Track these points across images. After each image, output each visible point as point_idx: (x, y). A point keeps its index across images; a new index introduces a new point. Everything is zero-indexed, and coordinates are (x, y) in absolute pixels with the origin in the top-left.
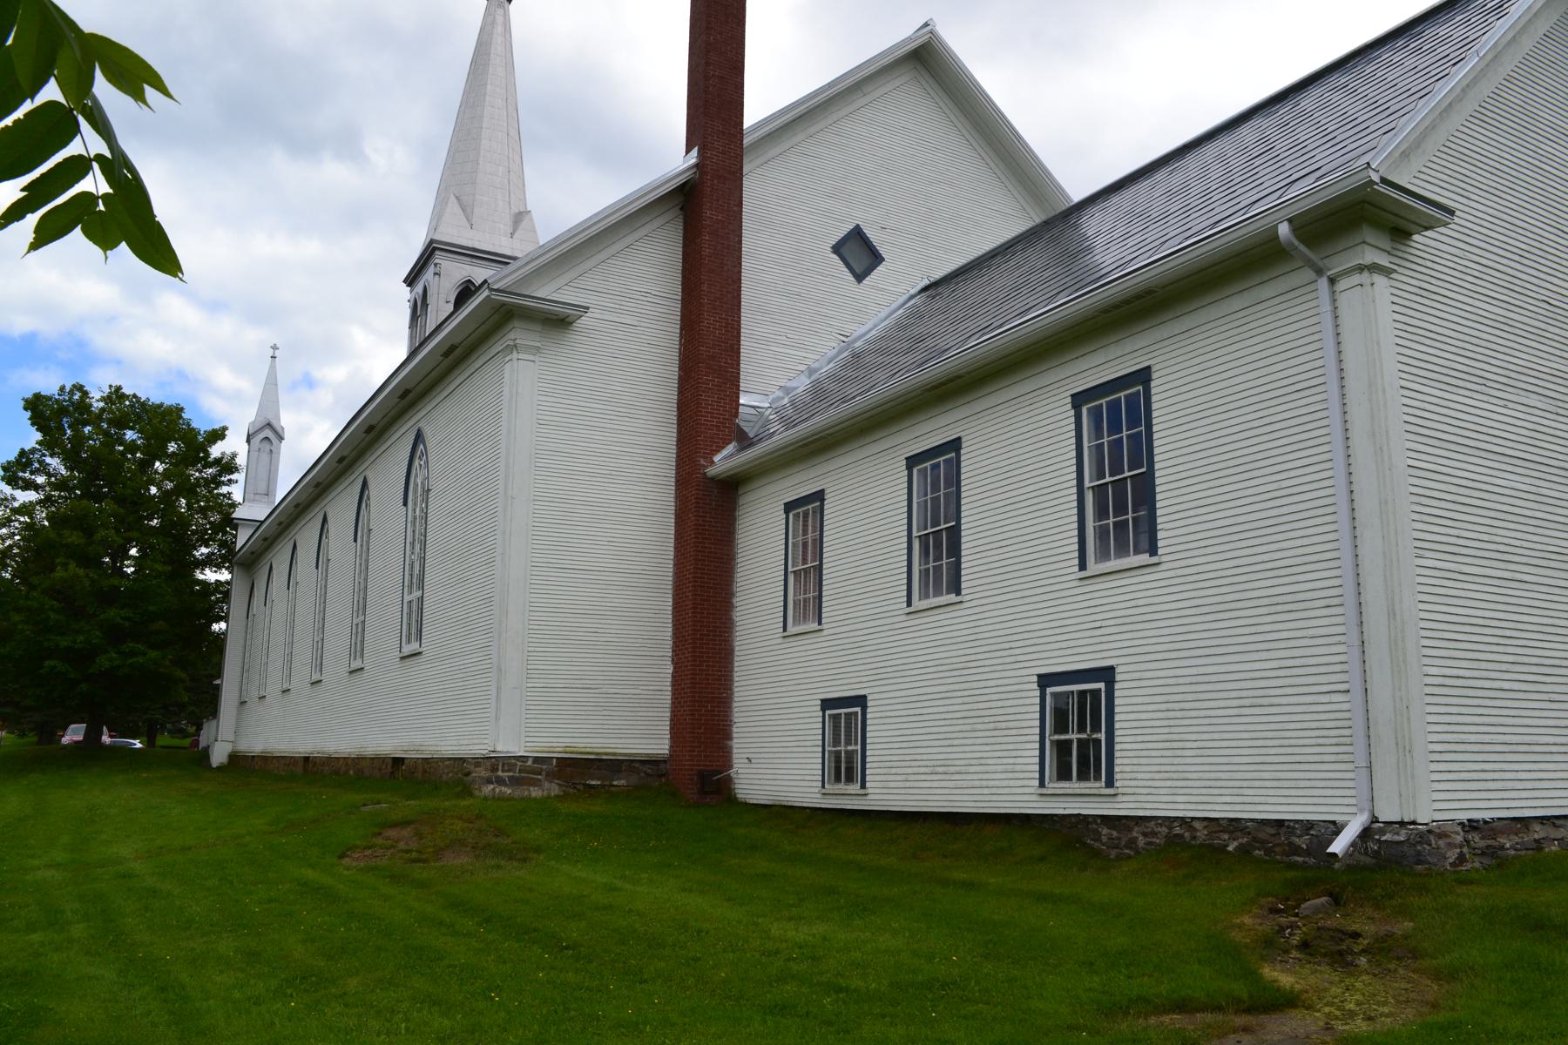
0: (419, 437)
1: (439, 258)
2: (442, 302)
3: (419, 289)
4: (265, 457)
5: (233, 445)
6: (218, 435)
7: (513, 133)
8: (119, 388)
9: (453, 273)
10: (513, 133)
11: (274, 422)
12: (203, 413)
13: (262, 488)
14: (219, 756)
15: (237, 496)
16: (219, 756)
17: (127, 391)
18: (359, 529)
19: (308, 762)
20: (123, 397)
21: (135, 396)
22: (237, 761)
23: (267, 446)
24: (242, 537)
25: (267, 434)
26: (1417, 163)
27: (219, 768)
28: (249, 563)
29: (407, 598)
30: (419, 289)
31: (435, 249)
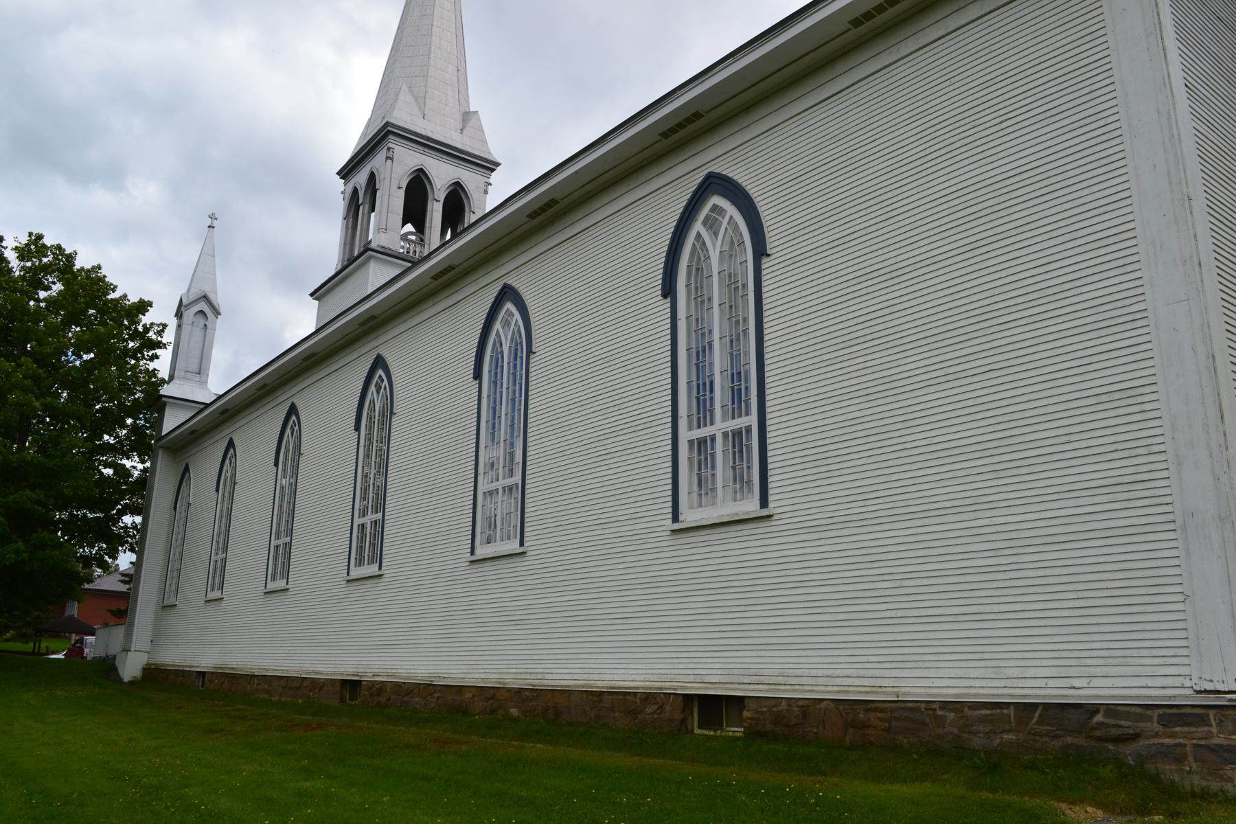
0: (231, 444)
1: (392, 142)
2: (394, 187)
3: (361, 178)
4: (198, 333)
5: (160, 314)
6: (143, 306)
7: (460, 36)
8: (40, 237)
9: (406, 160)
10: (460, 36)
11: (211, 295)
12: (127, 285)
13: (194, 365)
14: (130, 668)
15: (164, 373)
16: (130, 668)
17: (48, 241)
18: (226, 484)
19: (351, 686)
20: (42, 250)
21: (59, 247)
22: (155, 675)
23: (201, 321)
24: (172, 421)
25: (200, 309)
26: (351, 573)
27: (133, 683)
28: (184, 445)
29: (357, 521)
30: (361, 178)
31: (390, 132)
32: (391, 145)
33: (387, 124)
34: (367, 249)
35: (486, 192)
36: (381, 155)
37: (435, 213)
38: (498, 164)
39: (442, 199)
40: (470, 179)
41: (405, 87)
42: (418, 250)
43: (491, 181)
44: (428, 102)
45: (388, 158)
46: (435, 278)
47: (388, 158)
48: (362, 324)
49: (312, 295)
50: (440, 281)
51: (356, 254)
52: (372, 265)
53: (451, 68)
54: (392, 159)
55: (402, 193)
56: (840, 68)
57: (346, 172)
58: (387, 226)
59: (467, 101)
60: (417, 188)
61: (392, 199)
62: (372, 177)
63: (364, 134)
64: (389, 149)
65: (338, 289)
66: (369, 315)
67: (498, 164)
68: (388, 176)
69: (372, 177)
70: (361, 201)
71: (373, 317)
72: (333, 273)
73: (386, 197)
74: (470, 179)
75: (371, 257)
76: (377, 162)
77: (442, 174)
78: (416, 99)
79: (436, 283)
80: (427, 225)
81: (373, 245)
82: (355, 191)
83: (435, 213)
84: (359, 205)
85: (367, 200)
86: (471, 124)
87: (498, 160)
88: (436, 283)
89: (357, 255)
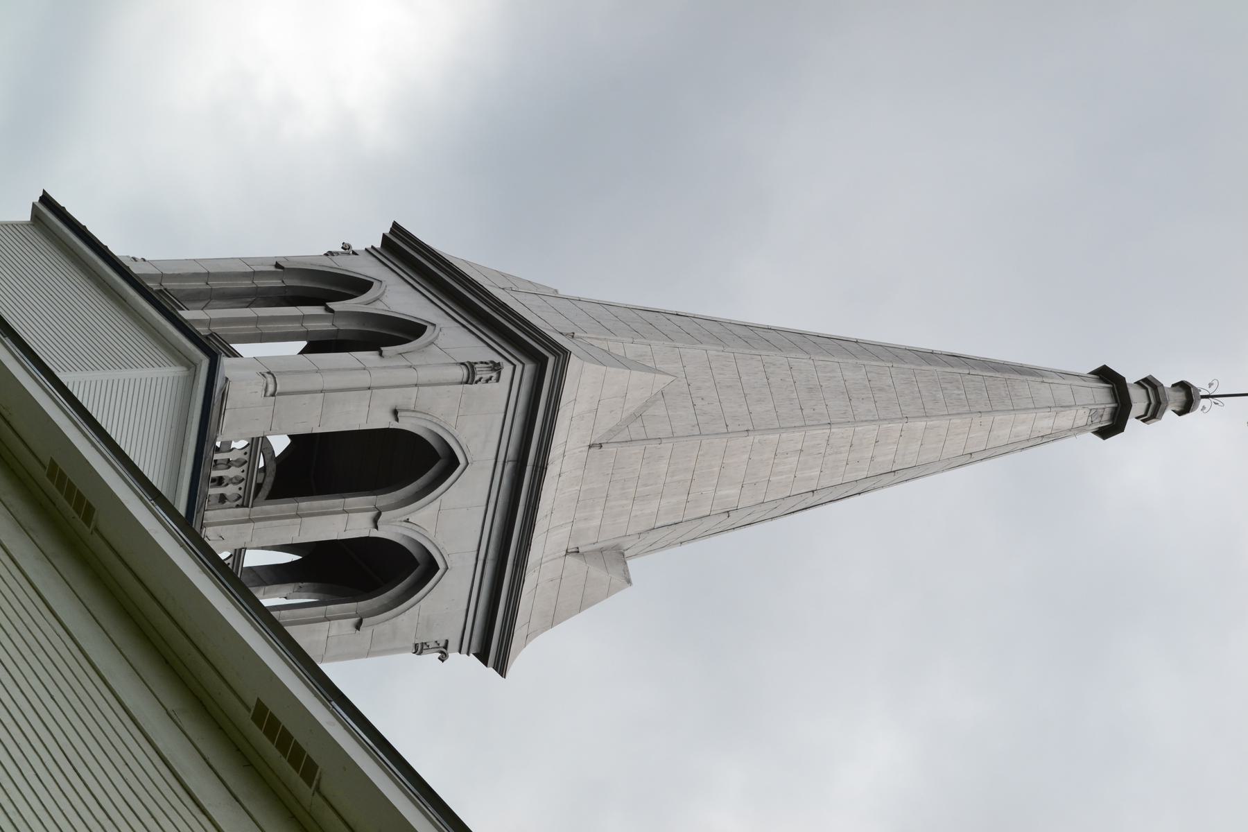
2: (396, 398)
3: (398, 297)
9: (475, 422)
10: (811, 500)
30: (398, 297)
31: (541, 362)
32: (507, 370)
33: (563, 355)
34: (214, 348)
35: (419, 649)
36: (476, 349)
37: (342, 520)
38: (501, 668)
39: (384, 532)
40: (450, 599)
41: (662, 381)
42: (230, 490)
43: (453, 656)
44: (636, 449)
45: (471, 367)
46: (261, 714)
47: (471, 367)
48: (54, 470)
49: (46, 199)
50: (258, 735)
51: (186, 315)
52: (172, 372)
53: (730, 493)
54: (470, 379)
55: (382, 421)
56: (300, 736)
57: (401, 248)
58: (281, 389)
59: (651, 549)
60: (403, 460)
61: (357, 393)
62: (409, 331)
63: (514, 284)
64: (496, 367)
65: (78, 279)
66: (90, 497)
67: (501, 668)
68: (424, 375)
69: (409, 331)
70: (332, 305)
71: (87, 512)
72: (117, 250)
73: (363, 379)
74: (450, 599)
75: (191, 366)
76: (453, 340)
77: (450, 522)
78: (638, 416)
79: (245, 719)
80: (305, 505)
81: (225, 361)
82: (361, 286)
83: (342, 520)
84: (315, 298)
85: (343, 325)
86: (597, 573)
87: (514, 667)
88: (245, 719)
89: (179, 311)
